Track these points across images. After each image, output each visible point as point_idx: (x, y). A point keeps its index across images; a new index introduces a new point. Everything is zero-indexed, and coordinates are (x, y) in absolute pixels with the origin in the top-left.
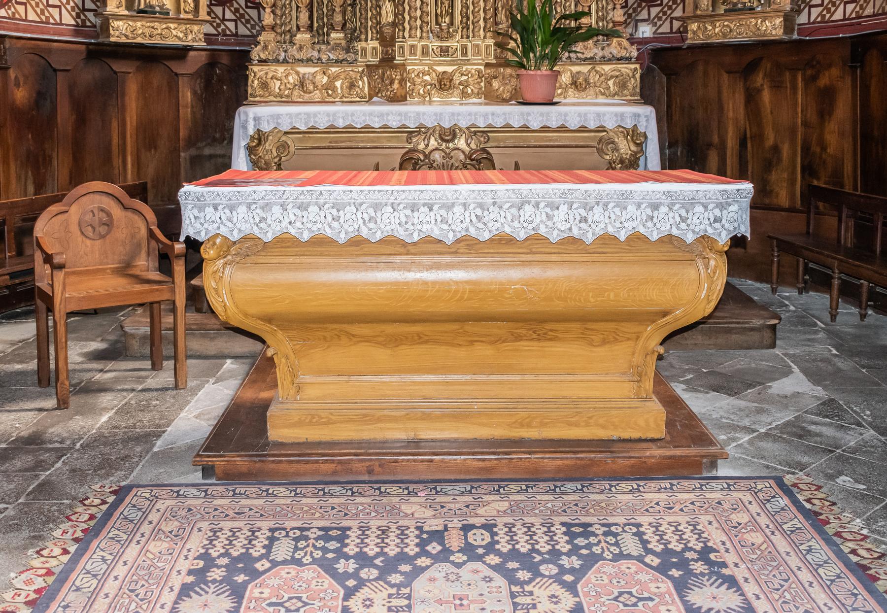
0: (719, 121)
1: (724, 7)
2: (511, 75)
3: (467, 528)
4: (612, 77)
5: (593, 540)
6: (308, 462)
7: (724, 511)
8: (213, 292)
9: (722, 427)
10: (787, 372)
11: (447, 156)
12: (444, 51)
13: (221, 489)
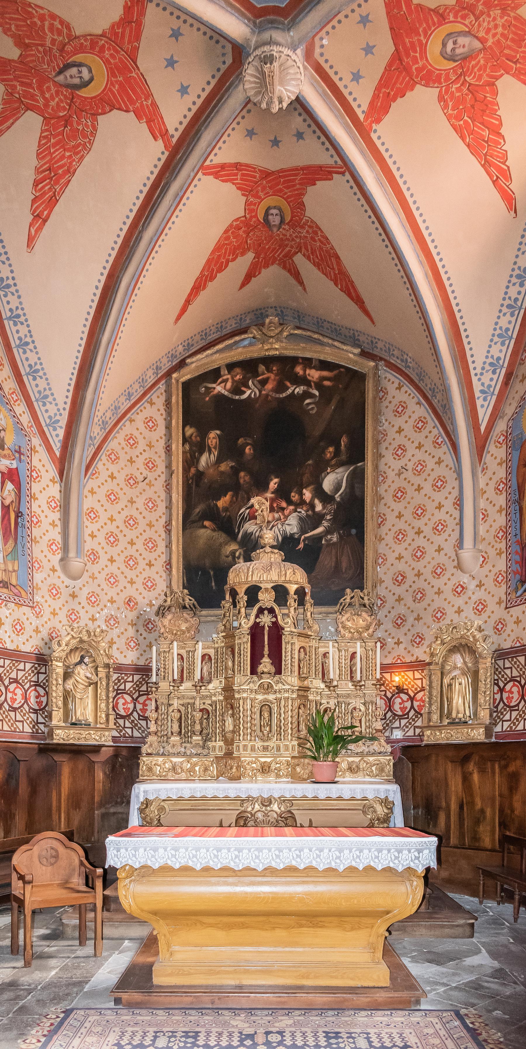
0: (446, 793)
1: (448, 721)
2: (308, 764)
3: (267, 1033)
4: (374, 765)
5: (340, 1040)
6: (176, 996)
7: (421, 1027)
8: (124, 898)
9: (429, 983)
10: (478, 952)
11: (266, 815)
12: (265, 748)
13: (125, 1011)
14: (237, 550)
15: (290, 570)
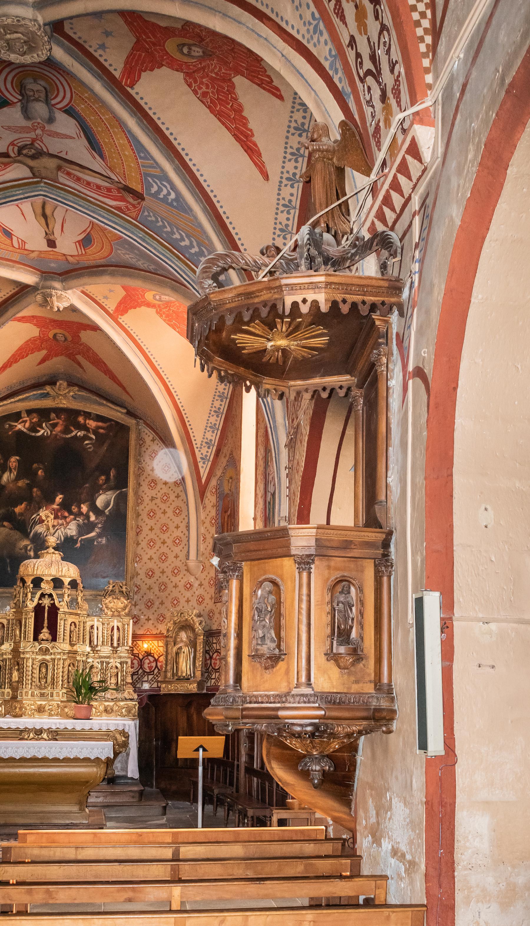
12: (42, 695)
14: (28, 545)
15: (66, 568)
